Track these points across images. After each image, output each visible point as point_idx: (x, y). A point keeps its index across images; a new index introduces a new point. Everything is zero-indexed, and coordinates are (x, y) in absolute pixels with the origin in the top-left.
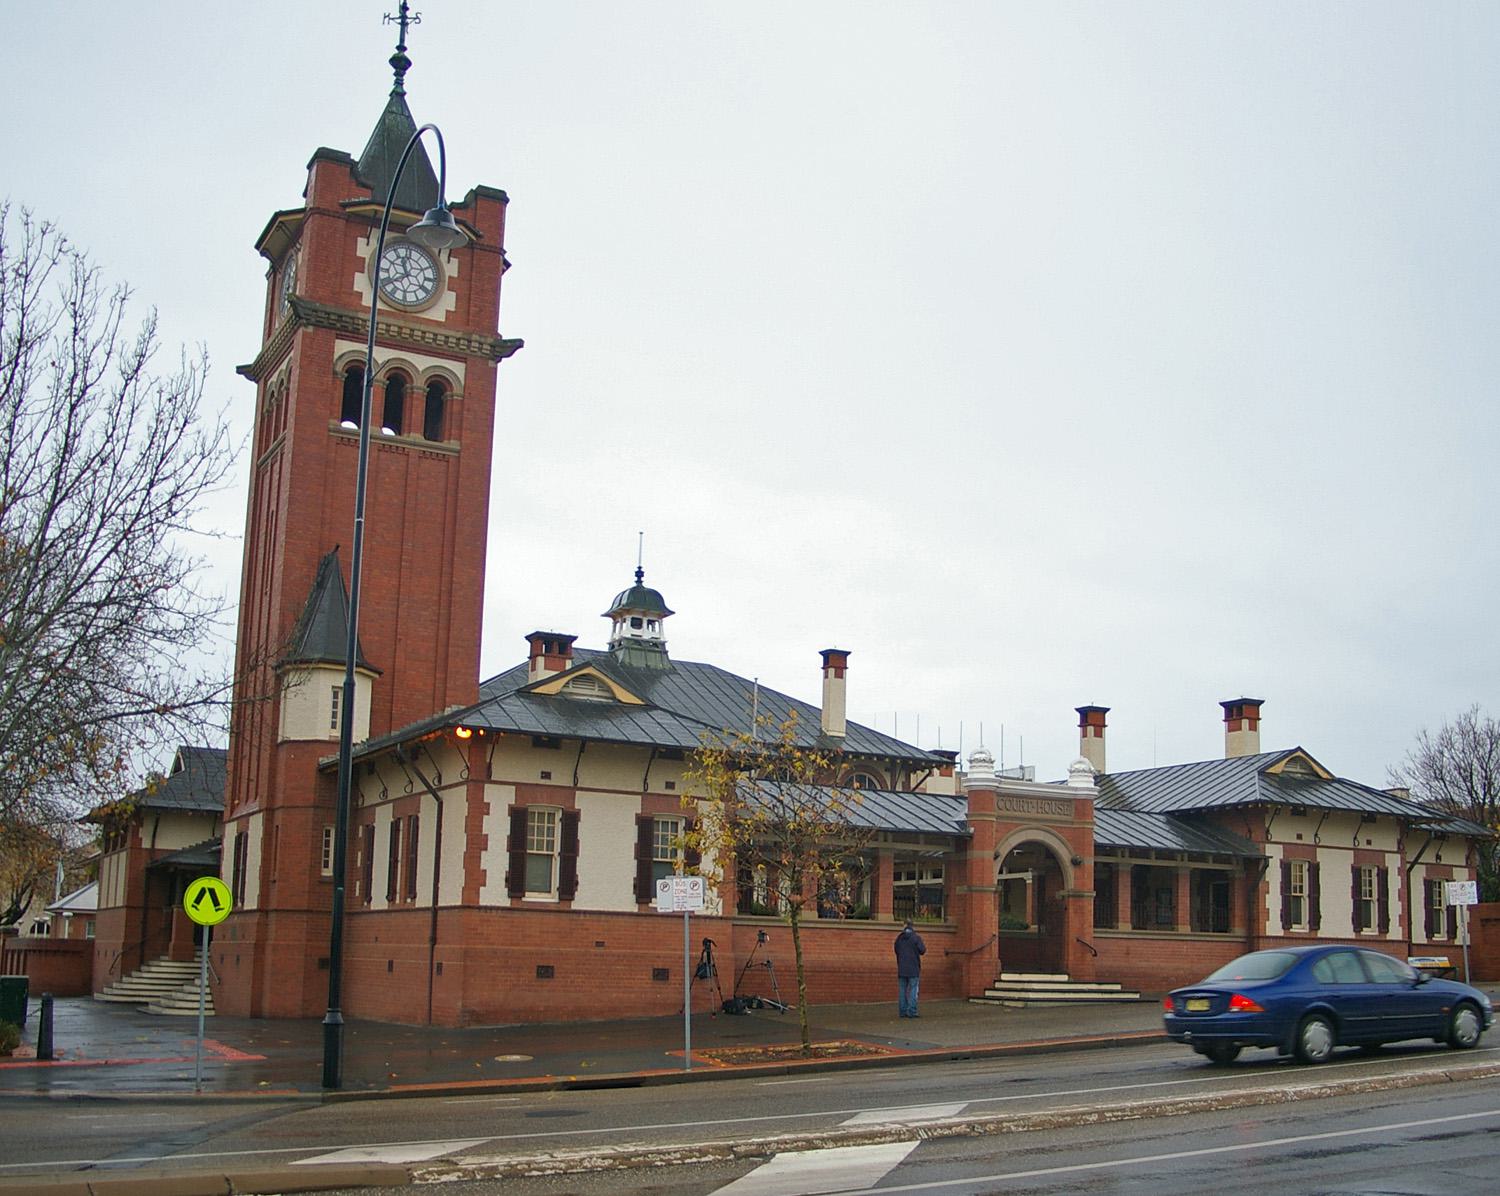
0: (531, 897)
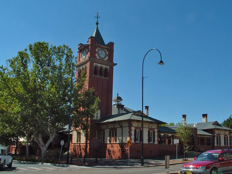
0: (137, 142)
